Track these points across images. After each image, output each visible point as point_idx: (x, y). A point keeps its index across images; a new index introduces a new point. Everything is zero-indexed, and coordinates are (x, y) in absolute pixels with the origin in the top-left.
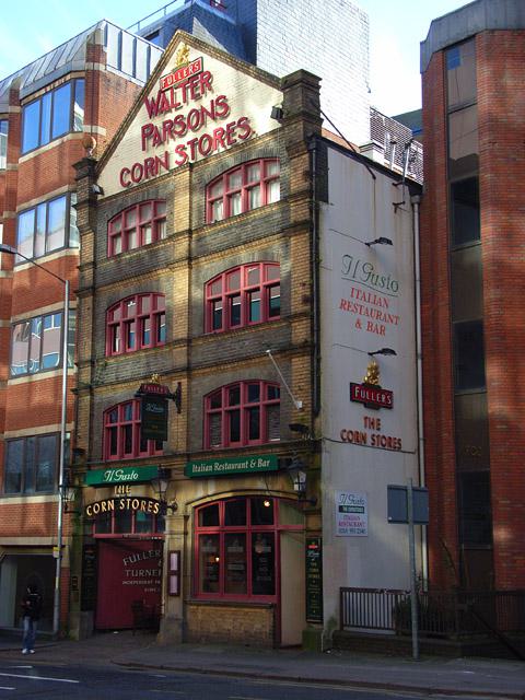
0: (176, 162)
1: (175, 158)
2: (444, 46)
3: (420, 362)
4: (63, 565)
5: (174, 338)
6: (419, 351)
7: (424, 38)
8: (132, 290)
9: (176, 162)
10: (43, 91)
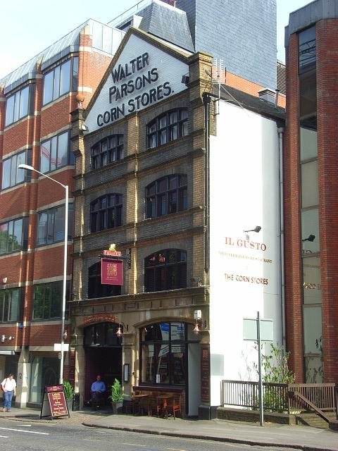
0: (129, 111)
1: (128, 108)
2: (297, 29)
3: (282, 235)
4: (65, 364)
5: (127, 223)
6: (282, 229)
7: (287, 24)
8: (104, 192)
9: (129, 111)
10: (55, 65)
